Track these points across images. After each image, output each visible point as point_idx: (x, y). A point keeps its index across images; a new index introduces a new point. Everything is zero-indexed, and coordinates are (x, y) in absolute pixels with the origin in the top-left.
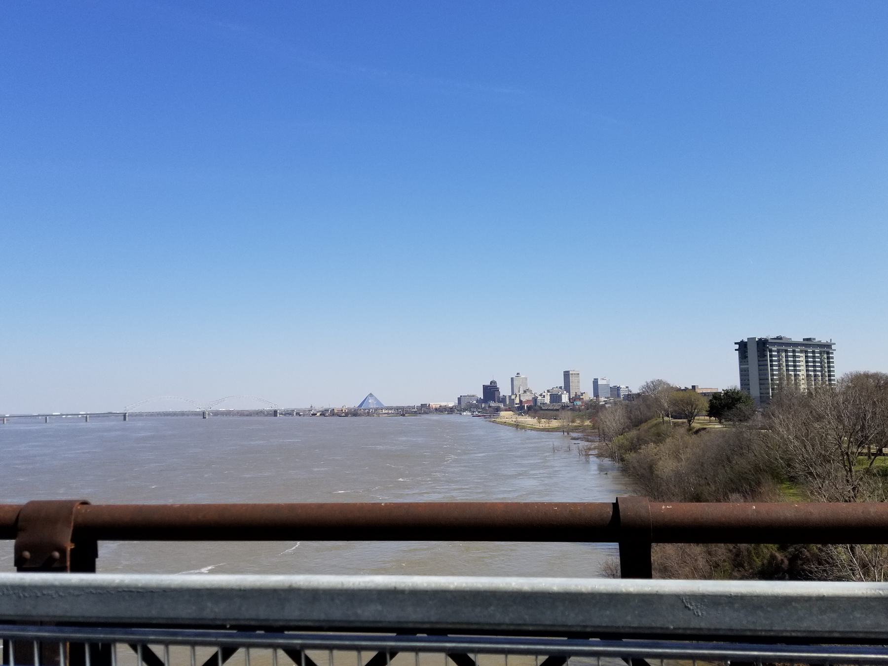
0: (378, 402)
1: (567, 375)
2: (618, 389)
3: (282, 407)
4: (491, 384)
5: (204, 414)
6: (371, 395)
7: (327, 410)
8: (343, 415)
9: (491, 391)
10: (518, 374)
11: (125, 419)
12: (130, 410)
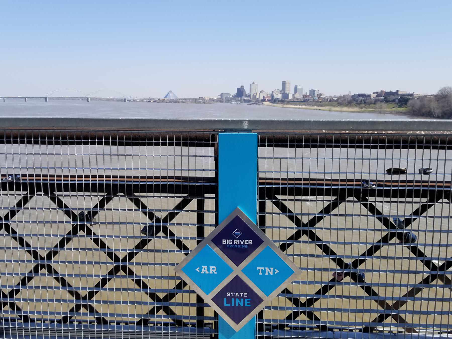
0: (175, 96)
1: (284, 83)
2: (314, 91)
3: (128, 97)
4: (241, 87)
5: (87, 99)
6: (171, 91)
7: (151, 99)
8: (168, 102)
9: (240, 92)
10: (253, 82)
11: (46, 101)
12: (49, 96)
